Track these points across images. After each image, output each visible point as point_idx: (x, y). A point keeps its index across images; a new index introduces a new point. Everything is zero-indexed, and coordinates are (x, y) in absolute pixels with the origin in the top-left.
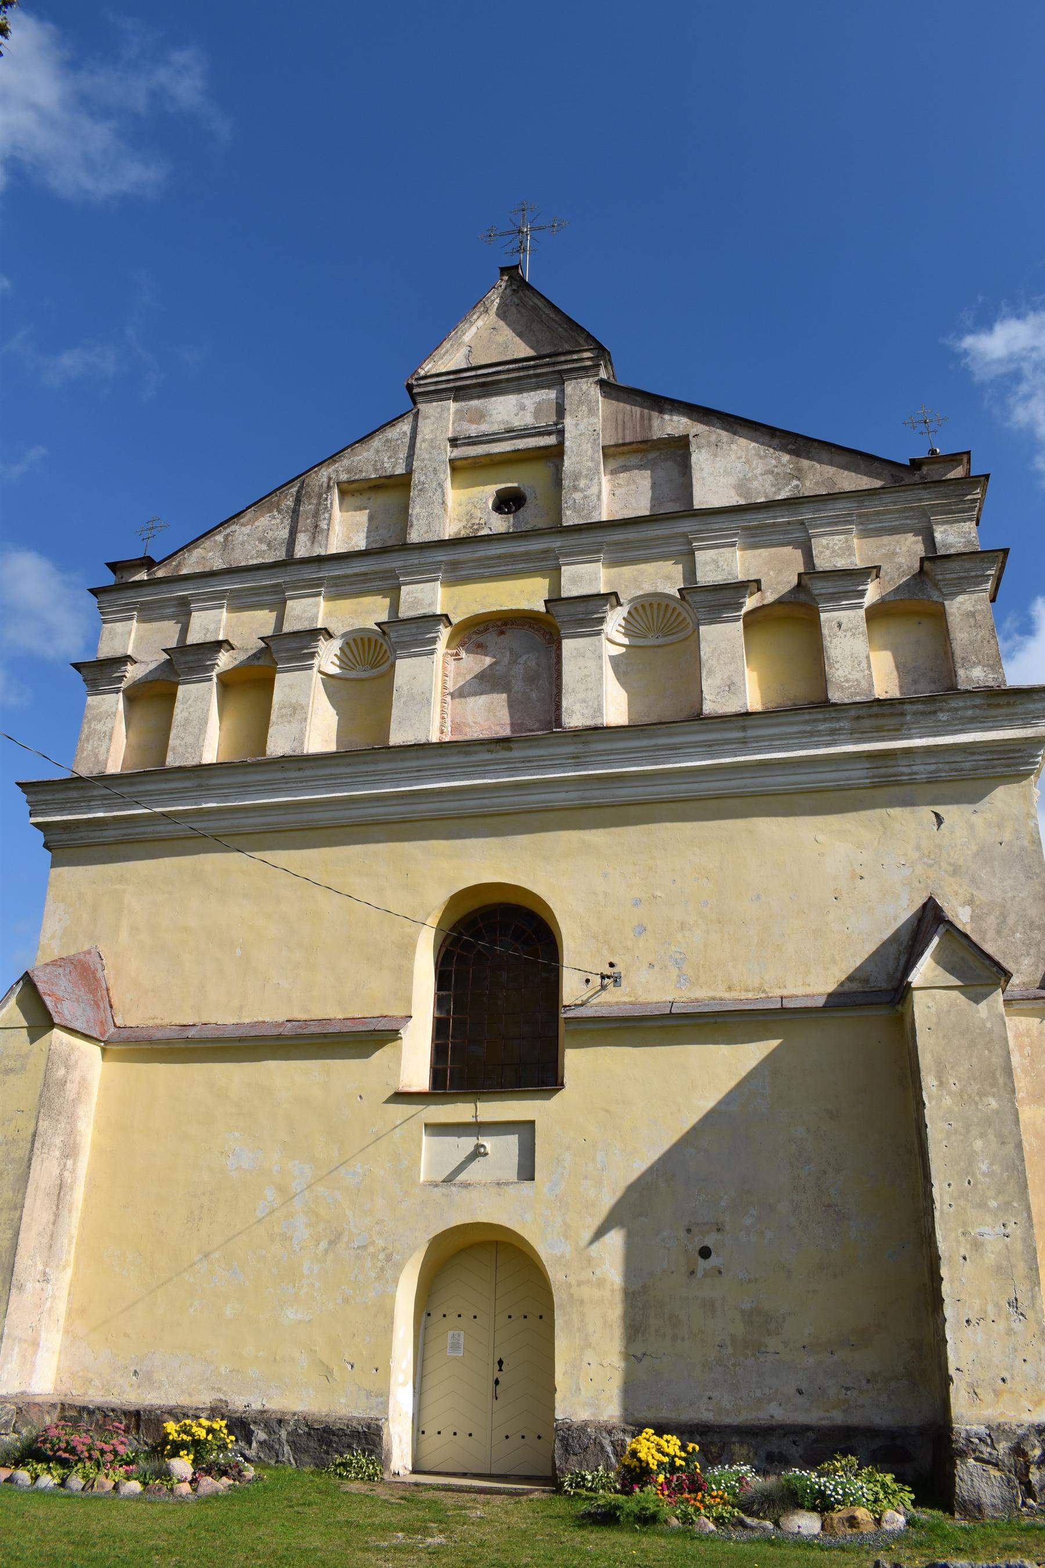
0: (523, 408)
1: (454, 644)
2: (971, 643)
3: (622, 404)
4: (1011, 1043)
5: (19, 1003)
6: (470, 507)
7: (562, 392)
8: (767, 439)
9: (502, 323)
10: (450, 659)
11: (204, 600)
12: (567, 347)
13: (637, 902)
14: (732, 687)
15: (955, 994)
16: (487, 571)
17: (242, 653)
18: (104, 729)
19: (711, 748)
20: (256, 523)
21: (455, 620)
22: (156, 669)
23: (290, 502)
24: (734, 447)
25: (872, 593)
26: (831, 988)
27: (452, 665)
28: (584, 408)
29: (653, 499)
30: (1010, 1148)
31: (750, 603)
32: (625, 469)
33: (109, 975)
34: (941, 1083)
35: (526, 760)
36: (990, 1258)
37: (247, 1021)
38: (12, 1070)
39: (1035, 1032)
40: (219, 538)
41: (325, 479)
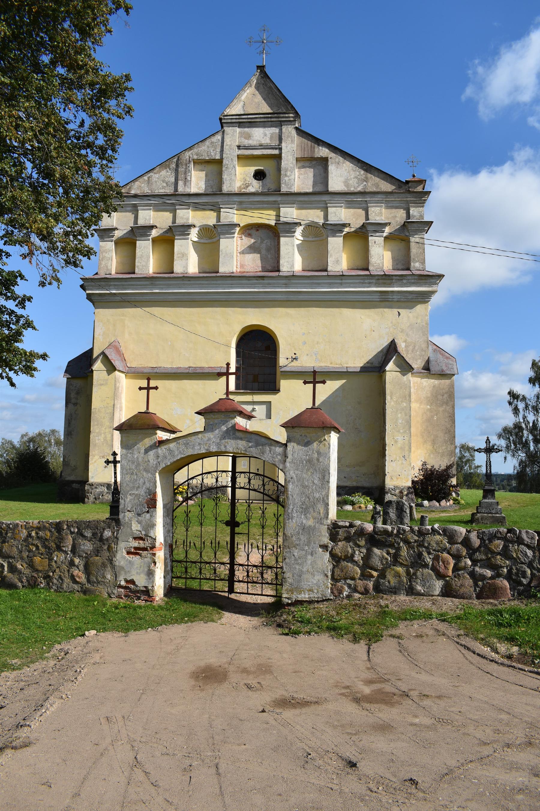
0: (266, 135)
1: (240, 233)
2: (417, 254)
3: (304, 139)
4: (412, 385)
5: (102, 362)
6: (245, 176)
7: (281, 130)
8: (357, 162)
9: (257, 92)
10: (239, 239)
11: (143, 206)
12: (284, 111)
13: (304, 334)
14: (338, 262)
15: (398, 373)
16: (253, 206)
17: (160, 230)
18: (108, 256)
19: (330, 285)
20: (161, 173)
21: (241, 225)
22: (126, 233)
23: (173, 166)
24: (344, 165)
25: (387, 230)
26: (362, 365)
27: (239, 241)
28: (290, 139)
29: (314, 181)
30: (408, 417)
31: (346, 230)
32: (304, 167)
33: (122, 349)
34: (391, 398)
35: (269, 284)
36: (399, 445)
37: (175, 367)
38: (102, 384)
39: (419, 382)
40: (146, 178)
41: (188, 157)
